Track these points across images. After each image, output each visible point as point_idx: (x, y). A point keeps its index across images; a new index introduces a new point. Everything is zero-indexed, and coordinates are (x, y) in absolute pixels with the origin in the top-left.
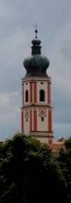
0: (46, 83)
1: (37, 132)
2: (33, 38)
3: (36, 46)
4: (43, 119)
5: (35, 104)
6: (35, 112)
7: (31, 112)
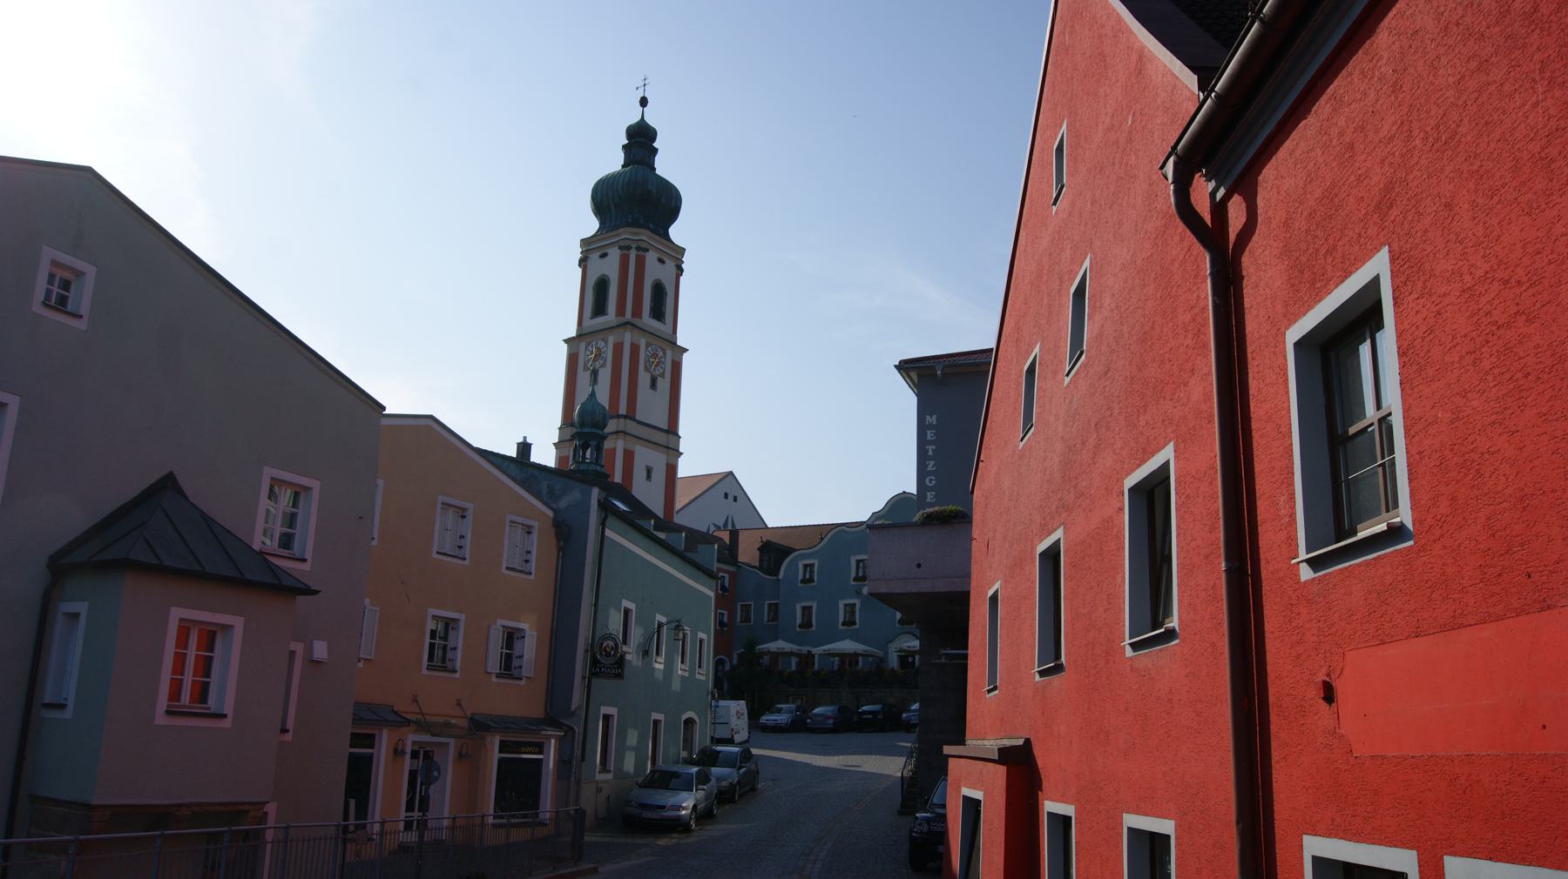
0: (670, 264)
1: (634, 420)
2: (642, 95)
3: (641, 140)
4: (653, 385)
5: (636, 321)
6: (635, 349)
7: (618, 348)
